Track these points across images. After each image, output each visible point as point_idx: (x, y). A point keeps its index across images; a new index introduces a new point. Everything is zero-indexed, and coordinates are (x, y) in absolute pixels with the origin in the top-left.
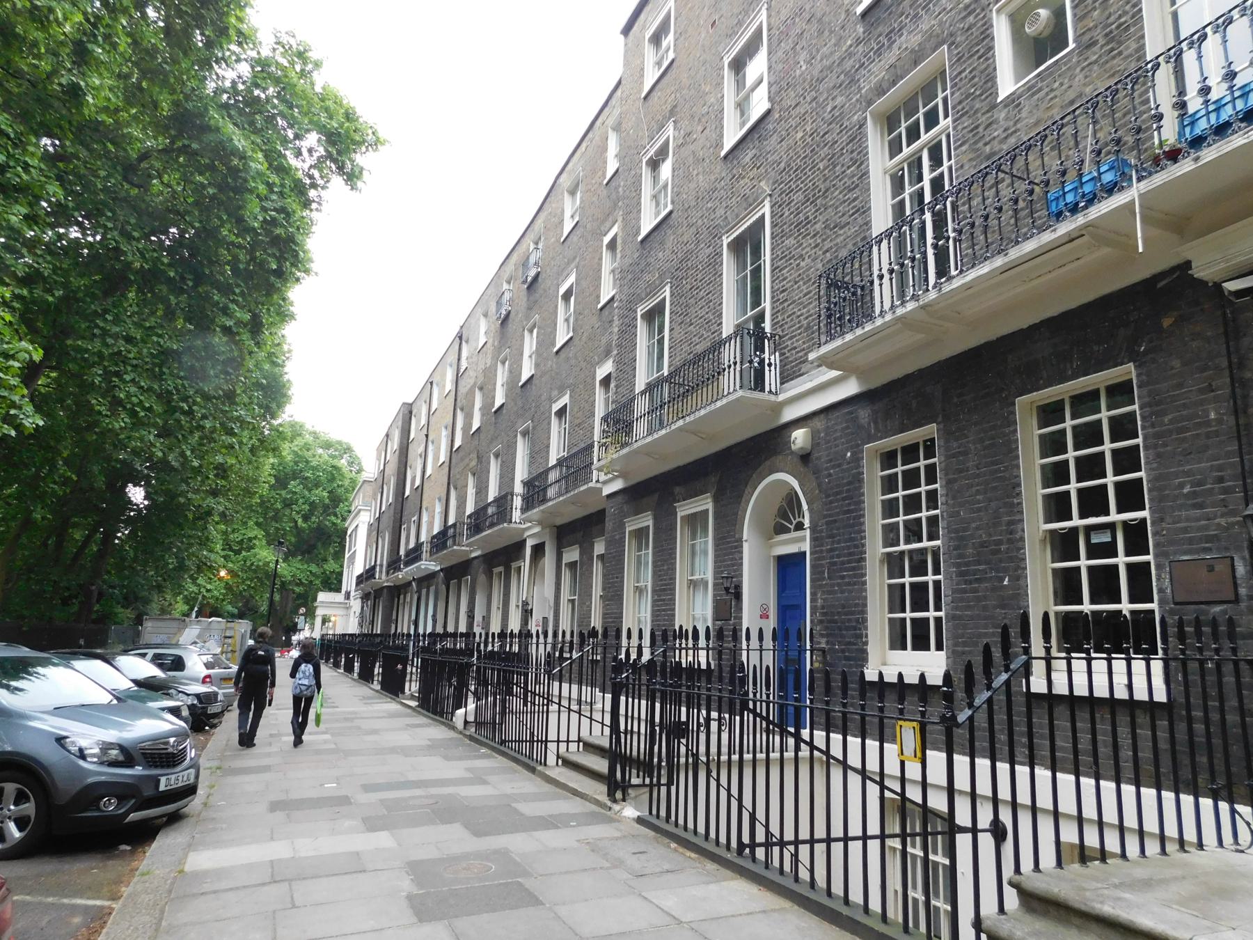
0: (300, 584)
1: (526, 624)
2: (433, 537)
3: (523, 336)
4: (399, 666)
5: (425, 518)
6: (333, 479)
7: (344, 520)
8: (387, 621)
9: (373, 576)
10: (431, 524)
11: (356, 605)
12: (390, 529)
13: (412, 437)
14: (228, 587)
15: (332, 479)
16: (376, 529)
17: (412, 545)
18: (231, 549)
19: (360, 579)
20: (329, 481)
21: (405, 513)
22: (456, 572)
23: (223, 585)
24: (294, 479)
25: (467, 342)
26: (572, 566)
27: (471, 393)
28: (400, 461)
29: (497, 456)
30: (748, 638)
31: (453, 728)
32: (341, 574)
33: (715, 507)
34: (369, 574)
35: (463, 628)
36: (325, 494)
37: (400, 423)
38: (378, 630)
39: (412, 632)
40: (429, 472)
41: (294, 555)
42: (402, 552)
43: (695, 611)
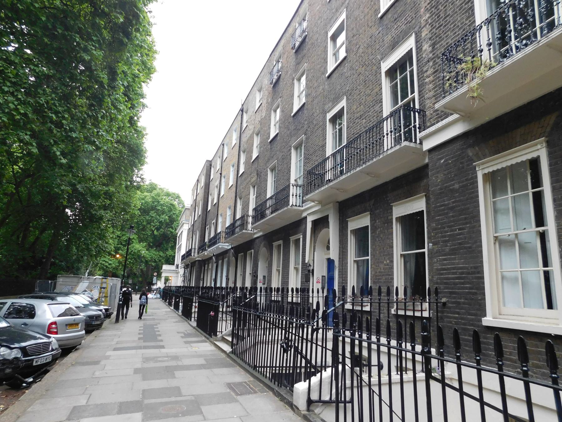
0: (155, 261)
1: (308, 280)
2: (227, 228)
3: (293, 84)
4: (212, 313)
5: (220, 220)
6: (171, 211)
7: (176, 230)
8: (198, 279)
9: (190, 255)
10: (225, 221)
11: (181, 271)
12: (200, 229)
13: (211, 178)
14: (120, 262)
15: (170, 210)
16: (192, 231)
17: (212, 235)
18: (121, 244)
19: (183, 257)
20: (169, 211)
21: (208, 219)
22: (243, 249)
23: (117, 261)
24: (153, 210)
25: (246, 113)
26: (361, 234)
27: (251, 138)
28: (205, 192)
29: (272, 170)
30: (313, 292)
31: (292, 406)
32: (174, 257)
33: (551, 155)
34: (189, 253)
35: (231, 285)
36: (167, 217)
37: (205, 172)
38: (193, 285)
39: (213, 286)
40: (222, 193)
41: (152, 247)
42: (206, 240)
43: (294, 282)
